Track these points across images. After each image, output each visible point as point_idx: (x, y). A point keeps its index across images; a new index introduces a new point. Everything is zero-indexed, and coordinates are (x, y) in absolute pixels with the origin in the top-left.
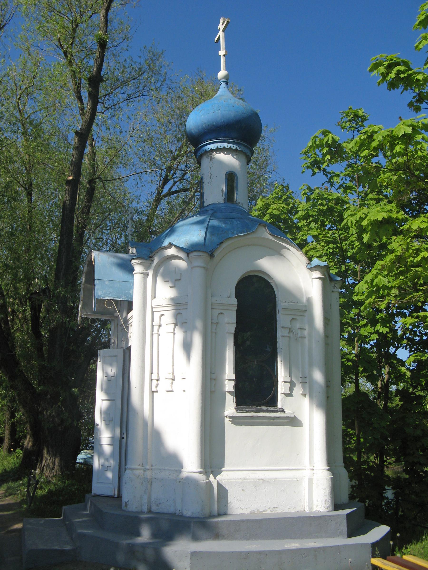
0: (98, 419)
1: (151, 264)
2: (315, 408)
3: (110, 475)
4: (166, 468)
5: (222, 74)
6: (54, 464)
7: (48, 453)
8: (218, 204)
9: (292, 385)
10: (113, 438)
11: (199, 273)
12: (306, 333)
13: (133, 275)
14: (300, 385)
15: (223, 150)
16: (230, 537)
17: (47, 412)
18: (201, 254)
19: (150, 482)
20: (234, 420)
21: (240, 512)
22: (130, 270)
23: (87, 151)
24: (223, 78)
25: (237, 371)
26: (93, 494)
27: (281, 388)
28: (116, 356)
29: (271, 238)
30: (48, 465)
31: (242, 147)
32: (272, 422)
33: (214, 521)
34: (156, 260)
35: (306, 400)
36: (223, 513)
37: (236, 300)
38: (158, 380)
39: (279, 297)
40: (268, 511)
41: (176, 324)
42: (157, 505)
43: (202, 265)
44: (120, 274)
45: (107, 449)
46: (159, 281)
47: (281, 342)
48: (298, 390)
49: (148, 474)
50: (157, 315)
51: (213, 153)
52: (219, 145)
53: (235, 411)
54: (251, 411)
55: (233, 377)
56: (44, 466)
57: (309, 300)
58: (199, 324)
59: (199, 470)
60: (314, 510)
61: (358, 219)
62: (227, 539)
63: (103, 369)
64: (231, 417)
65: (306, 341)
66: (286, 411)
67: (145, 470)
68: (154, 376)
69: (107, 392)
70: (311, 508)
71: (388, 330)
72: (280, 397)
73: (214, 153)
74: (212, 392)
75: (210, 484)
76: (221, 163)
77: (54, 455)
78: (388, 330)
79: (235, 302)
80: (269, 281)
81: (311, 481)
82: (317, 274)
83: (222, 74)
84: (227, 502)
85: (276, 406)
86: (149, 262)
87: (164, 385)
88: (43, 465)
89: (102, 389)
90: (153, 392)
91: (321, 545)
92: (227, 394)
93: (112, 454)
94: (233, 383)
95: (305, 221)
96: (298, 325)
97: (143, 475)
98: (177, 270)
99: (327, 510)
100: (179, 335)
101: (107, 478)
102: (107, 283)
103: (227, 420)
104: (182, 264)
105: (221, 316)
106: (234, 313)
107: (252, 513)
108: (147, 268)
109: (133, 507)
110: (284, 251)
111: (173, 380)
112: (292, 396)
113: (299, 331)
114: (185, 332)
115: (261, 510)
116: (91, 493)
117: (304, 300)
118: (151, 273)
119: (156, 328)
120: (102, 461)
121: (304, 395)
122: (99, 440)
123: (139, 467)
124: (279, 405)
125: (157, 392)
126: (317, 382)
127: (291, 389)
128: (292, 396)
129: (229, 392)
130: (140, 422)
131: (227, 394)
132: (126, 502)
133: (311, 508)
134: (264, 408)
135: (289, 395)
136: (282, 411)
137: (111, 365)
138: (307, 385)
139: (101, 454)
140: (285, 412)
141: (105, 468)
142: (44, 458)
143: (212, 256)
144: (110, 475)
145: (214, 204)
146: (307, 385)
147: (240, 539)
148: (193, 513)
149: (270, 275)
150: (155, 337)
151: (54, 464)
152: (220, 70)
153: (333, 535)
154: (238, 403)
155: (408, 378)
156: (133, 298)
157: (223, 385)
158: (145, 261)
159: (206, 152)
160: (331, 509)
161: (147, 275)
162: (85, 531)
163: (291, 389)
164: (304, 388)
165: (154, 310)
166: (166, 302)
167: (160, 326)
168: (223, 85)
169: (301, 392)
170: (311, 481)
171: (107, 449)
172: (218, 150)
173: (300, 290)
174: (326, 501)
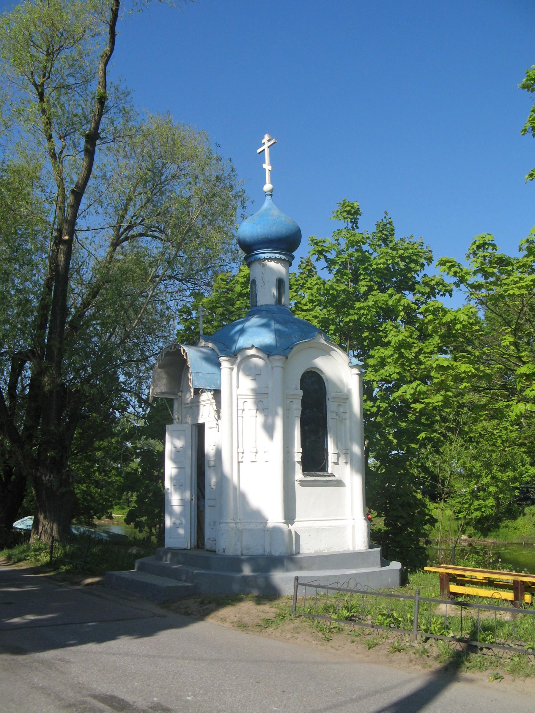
0: (168, 484)
1: (235, 361)
2: (354, 473)
3: (181, 531)
4: (253, 521)
5: (268, 187)
6: (52, 529)
7: (45, 518)
8: (270, 305)
9: (338, 455)
10: (182, 500)
11: (278, 372)
12: (347, 416)
13: (220, 369)
14: (344, 456)
15: (275, 259)
16: (309, 568)
17: (45, 476)
18: (281, 357)
19: (241, 532)
20: (303, 483)
21: (308, 551)
22: (219, 365)
23: (127, 232)
24: (269, 191)
25: (303, 446)
26: (166, 547)
27: (332, 458)
28: (184, 431)
29: (325, 342)
30: (46, 531)
31: (289, 257)
32: (327, 484)
33: (11, 623)
34: (239, 359)
35: (348, 468)
36: (298, 553)
37: (301, 391)
38: (243, 453)
39: (330, 393)
40: (326, 551)
41: (257, 410)
42: (248, 550)
43: (281, 365)
44: (209, 368)
45: (177, 509)
46: (241, 374)
47: (330, 423)
48: (342, 461)
49: (240, 526)
50: (241, 402)
51: (265, 260)
52: (271, 255)
53: (303, 476)
54: (313, 476)
55: (301, 450)
56: (41, 532)
57: (349, 391)
58: (280, 411)
59: (284, 521)
60: (356, 549)
61: (400, 339)
62: (307, 570)
63: (172, 443)
64: (300, 481)
65: (348, 422)
66: (336, 476)
67: (236, 523)
68: (240, 450)
69: (175, 460)
70: (354, 548)
71: (387, 405)
72: (330, 464)
73: (266, 261)
74: (288, 461)
75: (290, 531)
76: (271, 269)
77: (53, 521)
78: (387, 405)
79: (301, 392)
80: (321, 375)
81: (354, 527)
82: (356, 371)
83: (268, 187)
84: (299, 544)
85: (327, 472)
86: (234, 359)
87: (248, 457)
88: (40, 532)
89: (171, 459)
90: (239, 462)
91: (370, 571)
92: (296, 463)
93: (183, 514)
94: (301, 455)
95: (311, 304)
96: (342, 410)
97: (236, 527)
98: (256, 366)
99: (365, 549)
100: (260, 418)
101: (179, 534)
102: (200, 375)
103: (297, 483)
104: (259, 362)
105: (291, 403)
106: (301, 401)
107: (316, 552)
108: (233, 364)
109: (230, 552)
110: (332, 353)
111: (256, 453)
112: (338, 464)
113: (342, 414)
114: (266, 416)
115: (321, 550)
116: (164, 546)
117: (346, 390)
118: (235, 368)
119: (240, 412)
120: (173, 519)
121: (346, 463)
122: (170, 502)
123: (232, 521)
124: (330, 471)
125: (242, 462)
126: (355, 454)
127: (338, 459)
128: (338, 464)
129: (297, 462)
130: (231, 487)
131: (296, 463)
132: (224, 549)
133: (354, 548)
134: (321, 473)
135: (336, 463)
136: (332, 475)
137: (179, 438)
138: (349, 456)
139: (172, 514)
140: (334, 476)
141: (175, 526)
142: (41, 524)
143: (287, 358)
144: (181, 531)
145: (267, 305)
146: (349, 456)
147: (315, 570)
148: (281, 553)
149: (323, 371)
150: (240, 419)
151: (52, 529)
152: (265, 183)
153: (372, 566)
154: (304, 470)
155: (396, 445)
156: (220, 387)
157: (293, 457)
158: (232, 359)
159: (259, 259)
160: (368, 547)
161: (232, 369)
162: (203, 571)
163: (338, 459)
164: (346, 458)
165: (239, 397)
166: (249, 392)
167: (243, 410)
168: (269, 197)
169: (344, 461)
170: (354, 527)
171: (177, 509)
172: (270, 259)
173: (342, 382)
174: (364, 542)
